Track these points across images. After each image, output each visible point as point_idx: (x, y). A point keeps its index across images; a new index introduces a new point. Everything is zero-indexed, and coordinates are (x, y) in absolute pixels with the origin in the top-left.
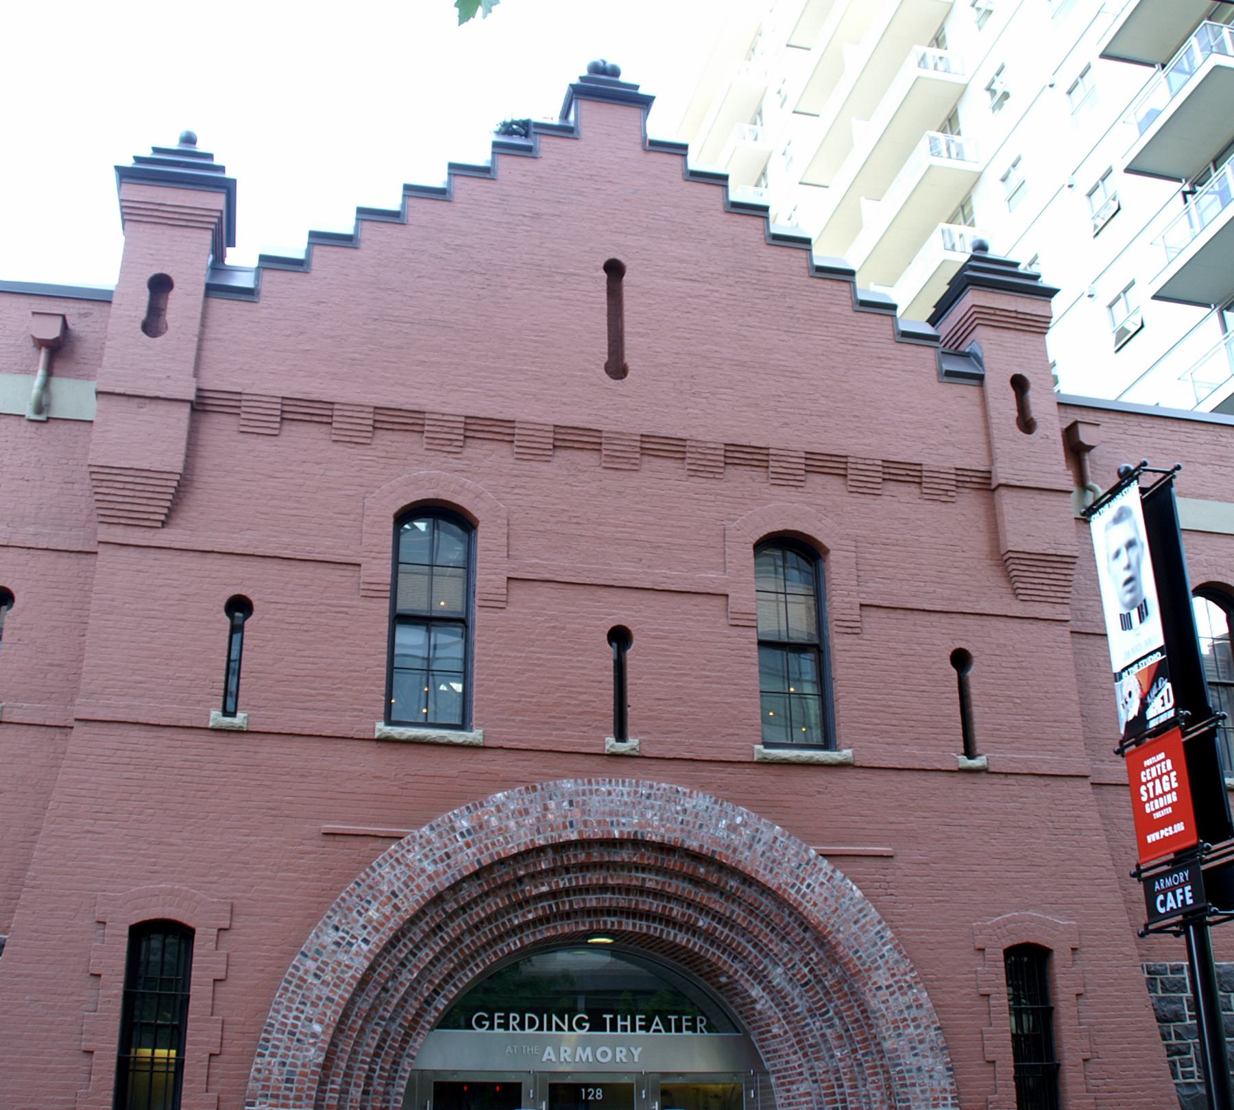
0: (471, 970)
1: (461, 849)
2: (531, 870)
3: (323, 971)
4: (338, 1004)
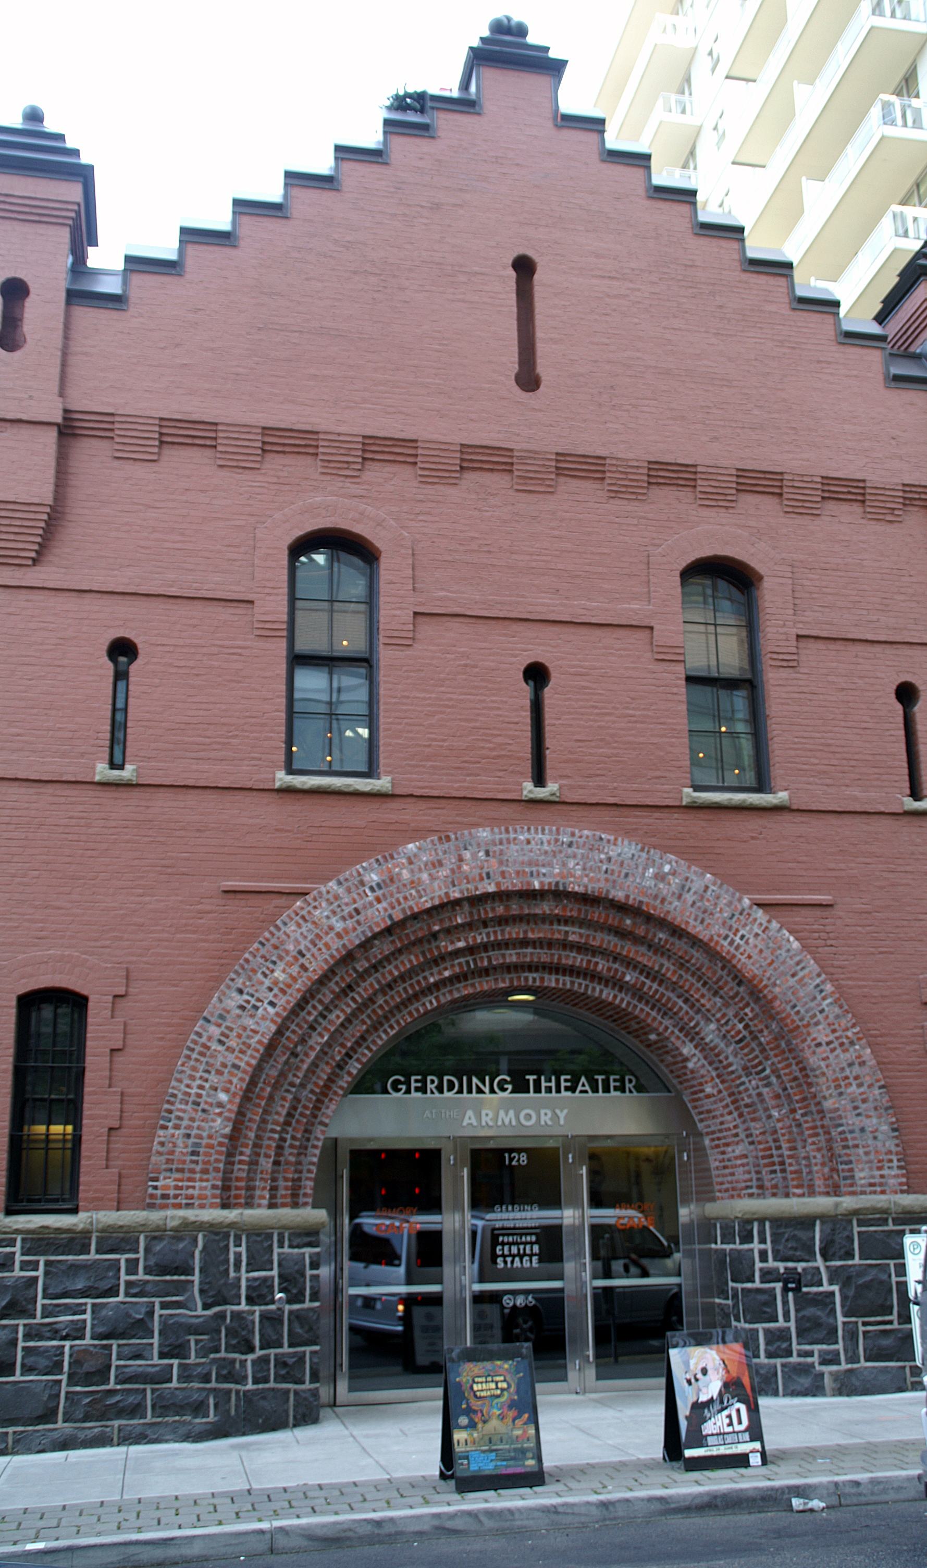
0: (385, 1032)
1: (371, 904)
2: (447, 924)
3: (227, 1037)
4: (245, 1072)
